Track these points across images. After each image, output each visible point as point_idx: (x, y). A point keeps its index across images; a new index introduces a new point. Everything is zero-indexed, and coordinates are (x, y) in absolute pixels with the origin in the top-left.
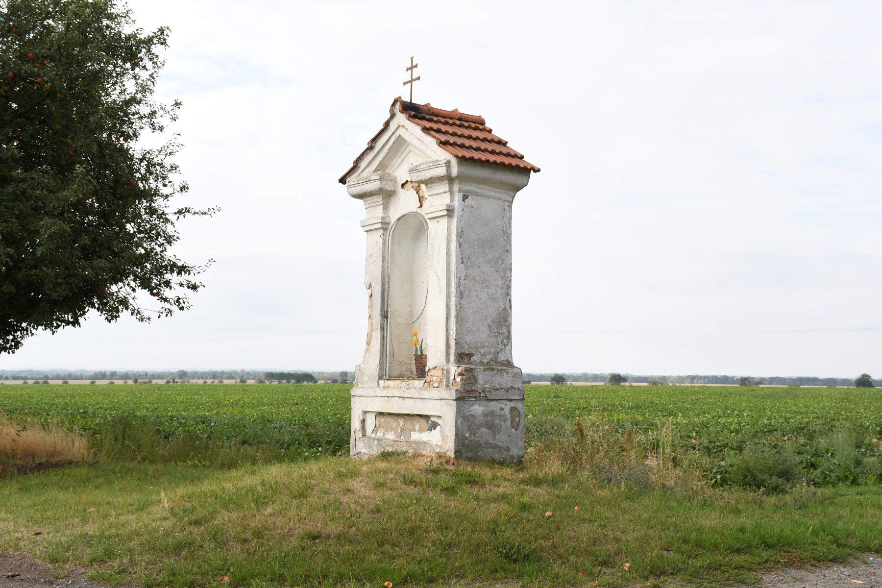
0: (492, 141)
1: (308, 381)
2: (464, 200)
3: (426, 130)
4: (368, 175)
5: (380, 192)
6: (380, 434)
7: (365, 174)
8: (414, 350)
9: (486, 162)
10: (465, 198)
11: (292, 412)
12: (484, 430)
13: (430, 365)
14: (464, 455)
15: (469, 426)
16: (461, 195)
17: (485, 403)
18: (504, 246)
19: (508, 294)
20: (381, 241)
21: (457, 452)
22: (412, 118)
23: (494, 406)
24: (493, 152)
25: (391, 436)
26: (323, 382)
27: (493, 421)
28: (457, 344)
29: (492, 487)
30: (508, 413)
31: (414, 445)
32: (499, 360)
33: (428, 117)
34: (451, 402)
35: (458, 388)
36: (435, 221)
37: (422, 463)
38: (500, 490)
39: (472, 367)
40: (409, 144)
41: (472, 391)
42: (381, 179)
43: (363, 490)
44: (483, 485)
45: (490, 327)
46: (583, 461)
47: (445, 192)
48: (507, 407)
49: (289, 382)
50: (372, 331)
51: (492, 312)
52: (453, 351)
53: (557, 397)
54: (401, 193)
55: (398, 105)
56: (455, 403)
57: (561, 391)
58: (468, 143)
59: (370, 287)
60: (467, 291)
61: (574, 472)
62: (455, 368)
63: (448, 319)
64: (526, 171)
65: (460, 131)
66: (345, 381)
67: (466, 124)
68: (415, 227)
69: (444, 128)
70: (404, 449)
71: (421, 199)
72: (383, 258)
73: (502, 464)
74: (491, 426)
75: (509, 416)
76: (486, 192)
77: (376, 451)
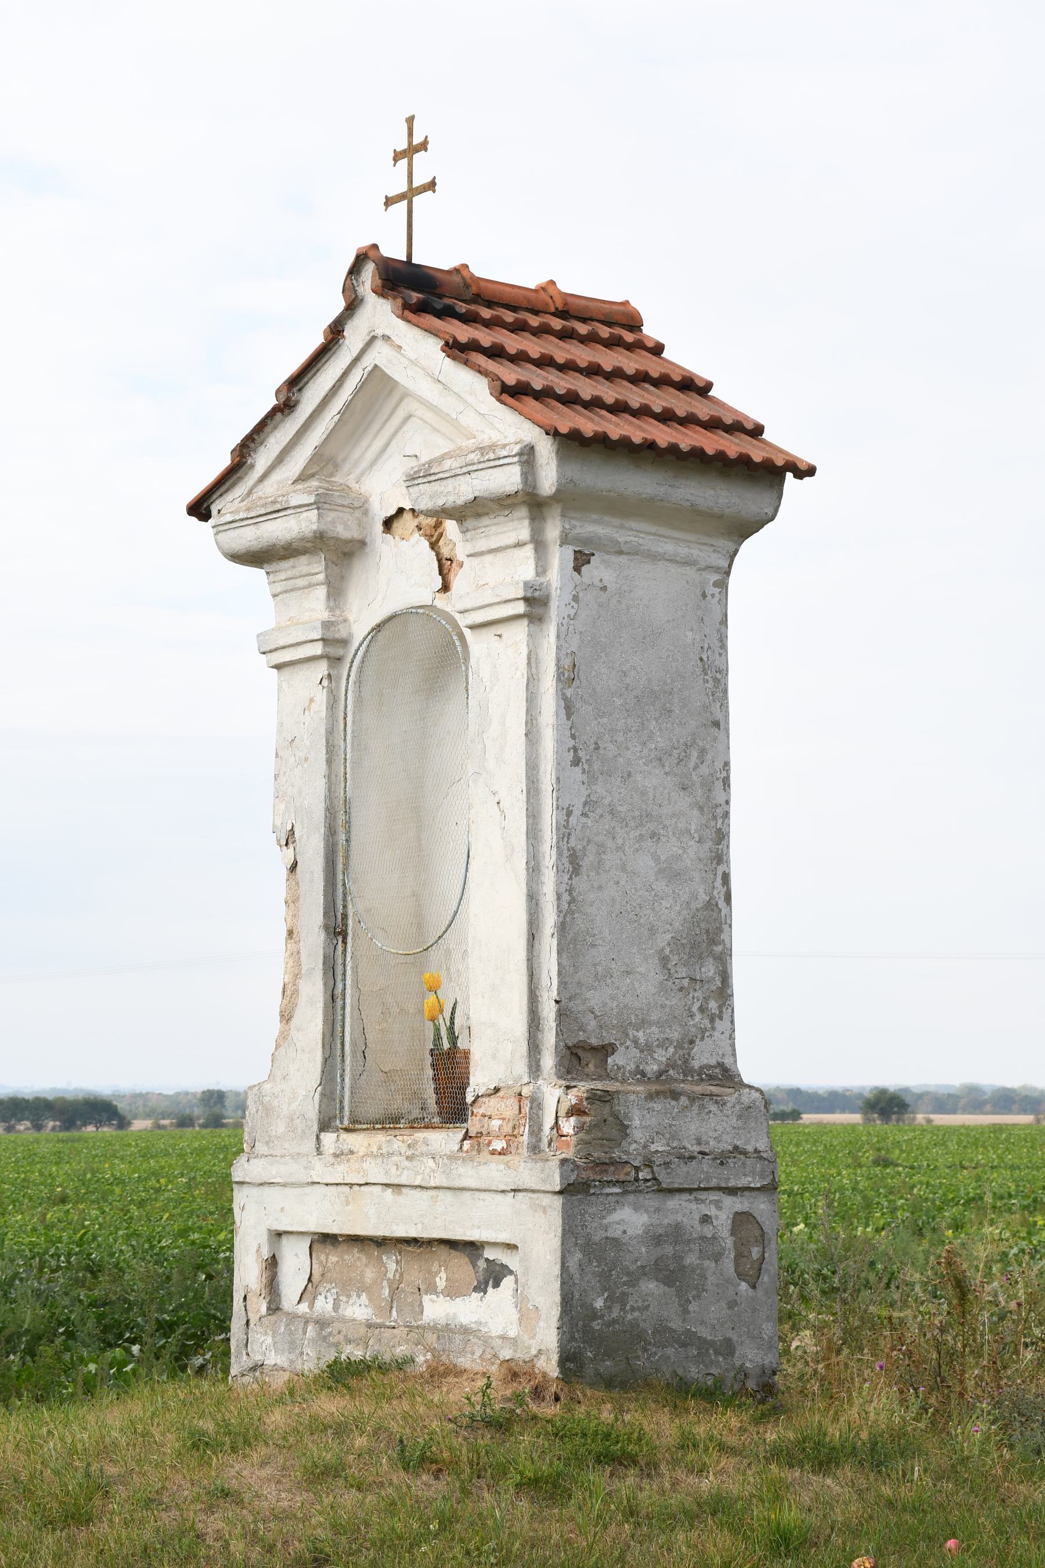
0: (662, 381)
1: (99, 1124)
2: (577, 569)
3: (456, 349)
4: (276, 493)
5: (318, 543)
6: (324, 1305)
7: (270, 488)
8: (431, 1035)
9: (645, 443)
10: (581, 560)
11: (49, 1227)
12: (650, 1286)
13: (479, 1081)
14: (589, 1370)
15: (605, 1276)
16: (569, 552)
17: (652, 1201)
18: (706, 708)
19: (720, 857)
20: (321, 697)
21: (568, 1359)
22: (412, 311)
23: (683, 1210)
24: (667, 417)
25: (359, 1310)
26: (147, 1123)
27: (678, 1258)
28: (562, 1015)
29: (680, 1474)
30: (725, 1232)
31: (431, 1338)
32: (696, 1064)
33: (462, 308)
34: (546, 1200)
35: (569, 1153)
36: (489, 633)
37: (456, 1395)
38: (707, 1484)
39: (612, 1086)
40: (406, 394)
41: (613, 1163)
42: (320, 504)
43: (269, 1491)
44: (650, 1469)
45: (664, 961)
46: (970, 1384)
47: (519, 545)
48: (724, 1211)
49: (38, 1128)
50: (297, 976)
51: (671, 914)
52: (549, 1038)
53: (885, 1163)
54: (384, 546)
55: (369, 271)
56: (558, 1202)
57: (897, 1144)
58: (587, 388)
59: (290, 839)
60: (592, 849)
61: (939, 1422)
62: (558, 1092)
63: (532, 938)
64: (771, 473)
65: (562, 351)
66: (215, 1121)
67: (583, 329)
68: (430, 652)
69: (513, 343)
70: (401, 1350)
71: (445, 567)
72: (331, 750)
73: (711, 1395)
74: (673, 1275)
75: (729, 1242)
76: (648, 542)
77: (311, 1360)
